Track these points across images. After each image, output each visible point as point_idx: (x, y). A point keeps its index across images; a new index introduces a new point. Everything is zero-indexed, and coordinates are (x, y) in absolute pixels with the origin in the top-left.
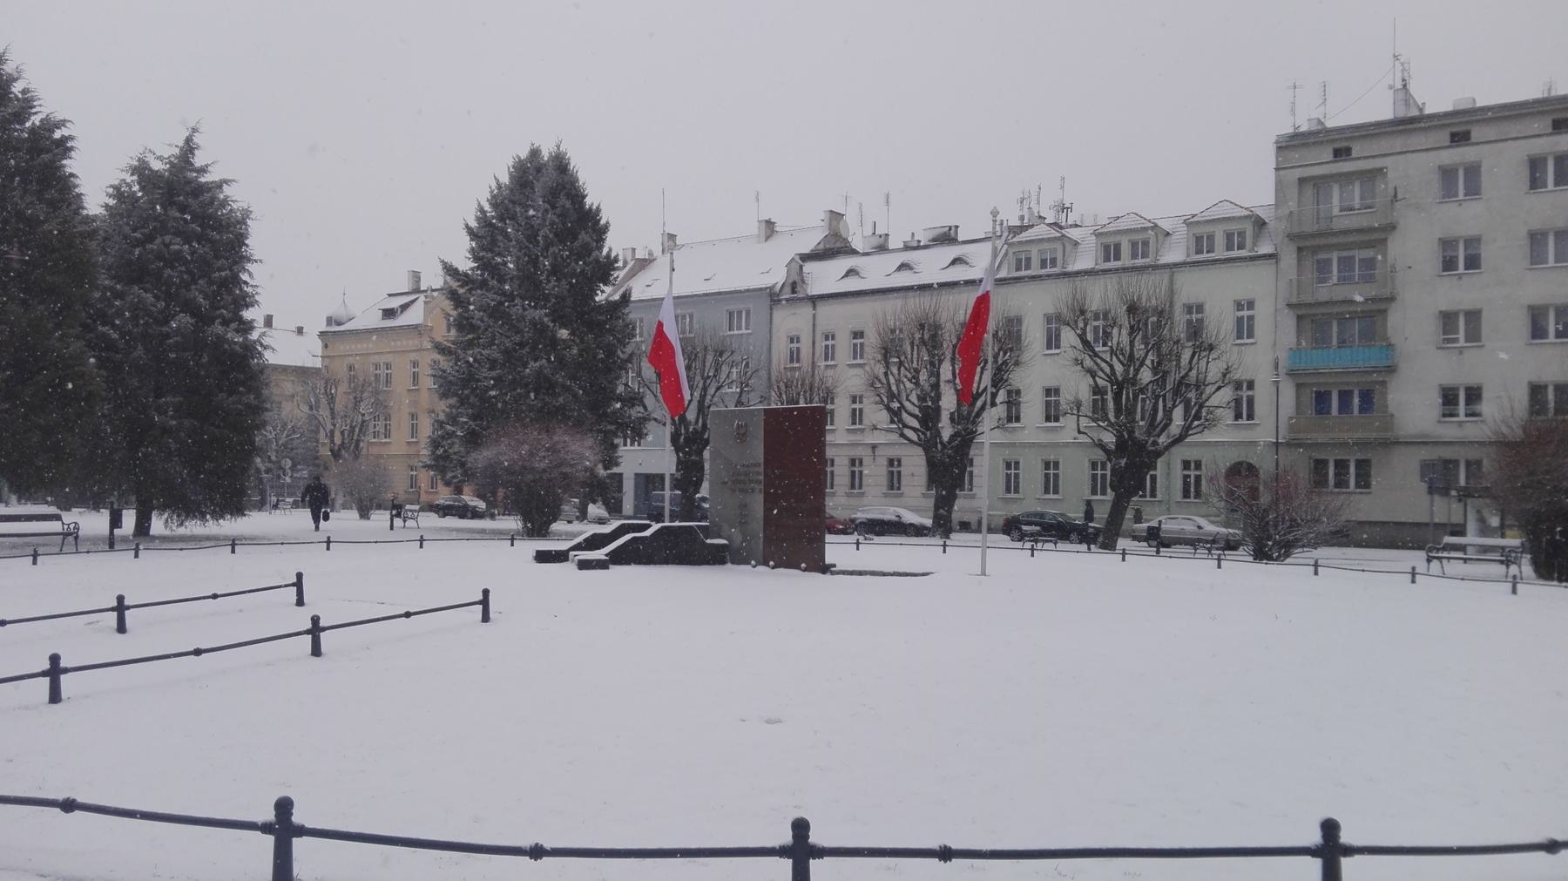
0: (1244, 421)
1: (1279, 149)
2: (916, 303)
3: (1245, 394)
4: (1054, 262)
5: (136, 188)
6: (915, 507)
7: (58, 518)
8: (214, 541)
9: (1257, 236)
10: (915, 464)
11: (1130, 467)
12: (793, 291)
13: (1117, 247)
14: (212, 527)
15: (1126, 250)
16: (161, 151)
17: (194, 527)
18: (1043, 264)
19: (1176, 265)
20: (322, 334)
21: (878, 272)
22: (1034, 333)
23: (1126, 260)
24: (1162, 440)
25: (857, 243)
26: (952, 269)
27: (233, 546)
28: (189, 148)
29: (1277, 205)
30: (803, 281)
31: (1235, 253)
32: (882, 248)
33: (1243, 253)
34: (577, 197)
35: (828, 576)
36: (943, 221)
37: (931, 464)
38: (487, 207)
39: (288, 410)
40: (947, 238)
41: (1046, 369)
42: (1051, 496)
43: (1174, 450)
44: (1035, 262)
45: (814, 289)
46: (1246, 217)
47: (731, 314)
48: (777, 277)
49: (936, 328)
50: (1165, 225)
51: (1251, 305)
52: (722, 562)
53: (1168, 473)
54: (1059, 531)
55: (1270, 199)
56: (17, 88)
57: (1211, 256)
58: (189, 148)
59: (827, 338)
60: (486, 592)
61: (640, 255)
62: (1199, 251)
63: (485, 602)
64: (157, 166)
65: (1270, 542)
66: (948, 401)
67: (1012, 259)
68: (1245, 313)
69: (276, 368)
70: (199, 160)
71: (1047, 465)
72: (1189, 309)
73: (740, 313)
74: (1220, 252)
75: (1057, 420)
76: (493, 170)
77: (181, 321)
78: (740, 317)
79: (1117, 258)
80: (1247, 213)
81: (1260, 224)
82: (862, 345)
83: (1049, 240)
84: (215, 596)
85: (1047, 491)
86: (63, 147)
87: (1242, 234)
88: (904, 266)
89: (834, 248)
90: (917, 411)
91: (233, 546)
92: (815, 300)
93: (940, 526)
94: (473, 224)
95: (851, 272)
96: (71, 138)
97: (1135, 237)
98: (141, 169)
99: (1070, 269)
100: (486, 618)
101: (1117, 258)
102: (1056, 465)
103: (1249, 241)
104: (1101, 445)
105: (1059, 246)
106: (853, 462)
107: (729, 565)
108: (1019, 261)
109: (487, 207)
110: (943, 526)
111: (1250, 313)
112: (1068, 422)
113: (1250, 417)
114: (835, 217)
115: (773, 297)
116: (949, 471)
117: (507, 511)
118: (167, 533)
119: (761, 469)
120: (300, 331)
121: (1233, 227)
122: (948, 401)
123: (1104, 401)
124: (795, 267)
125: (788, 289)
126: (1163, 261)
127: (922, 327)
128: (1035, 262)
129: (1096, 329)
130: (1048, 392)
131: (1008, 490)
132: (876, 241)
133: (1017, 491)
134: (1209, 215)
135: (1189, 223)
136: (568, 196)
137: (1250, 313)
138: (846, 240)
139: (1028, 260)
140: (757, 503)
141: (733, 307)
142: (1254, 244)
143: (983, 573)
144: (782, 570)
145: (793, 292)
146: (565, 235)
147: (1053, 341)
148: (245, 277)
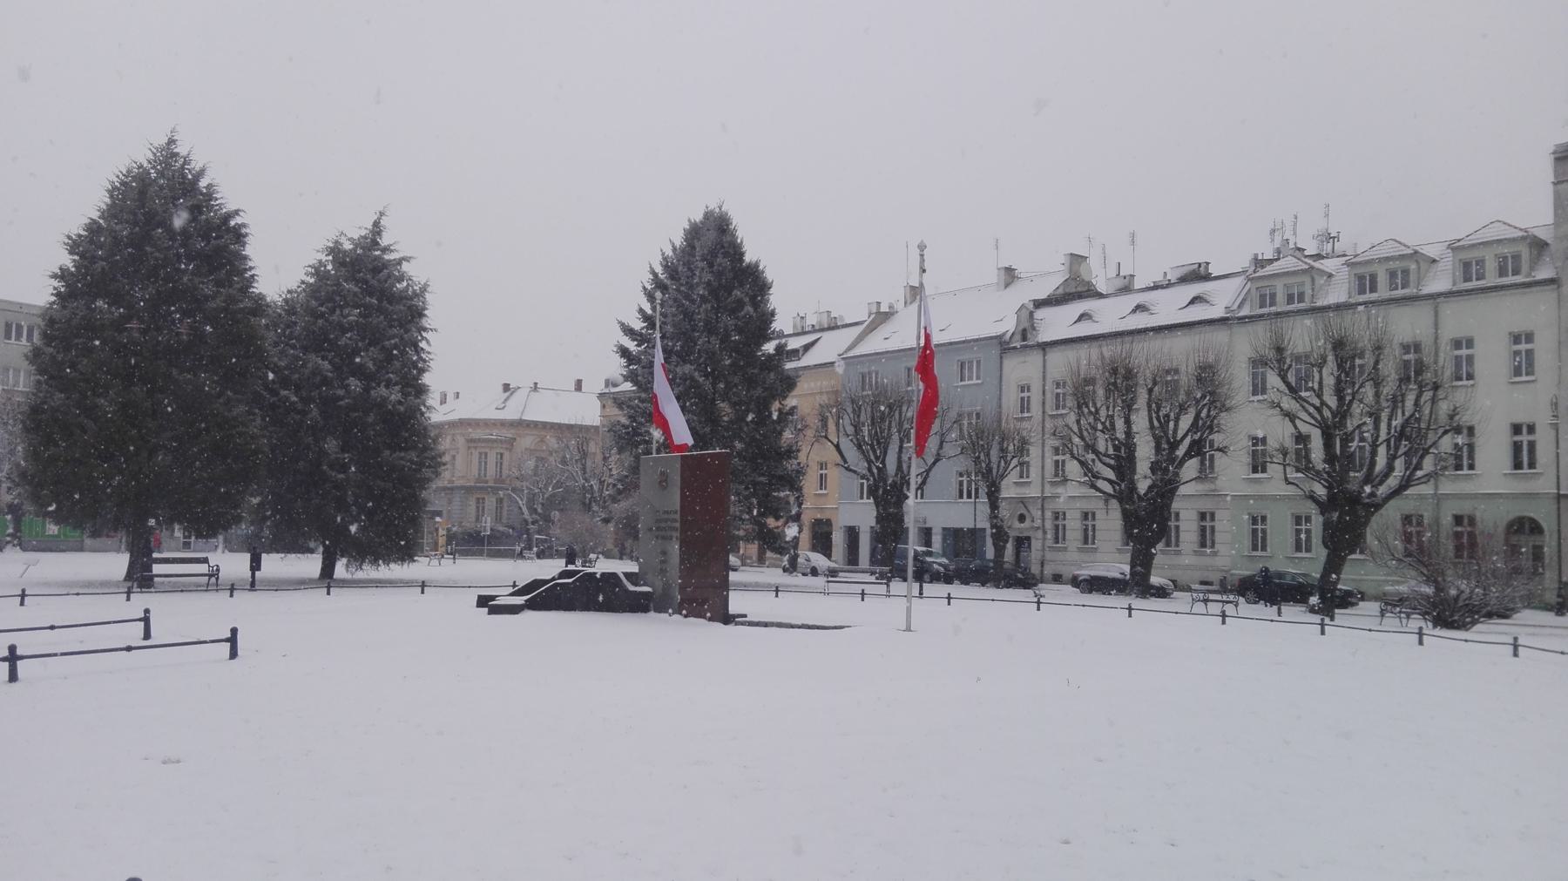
0: (1465, 472)
1: (1557, 159)
2: (1109, 350)
3: (1524, 438)
4: (1301, 298)
5: (330, 267)
6: (1119, 567)
7: (205, 561)
8: (407, 584)
9: (1535, 262)
10: (1111, 522)
11: (1345, 518)
12: (1024, 338)
13: (1373, 278)
14: (396, 571)
15: (1382, 280)
16: (354, 229)
17: (369, 572)
18: (1290, 299)
19: (1440, 295)
20: (601, 396)
21: (1111, 315)
22: (1239, 376)
23: (1383, 292)
24: (1382, 490)
25: (1102, 287)
26: (1192, 308)
27: (777, 591)
28: (377, 229)
29: (1557, 224)
30: (1034, 329)
31: (1510, 279)
32: (1126, 289)
33: (1519, 279)
34: (736, 252)
35: (731, 628)
36: (1191, 258)
37: (1126, 515)
38: (659, 270)
39: (459, 466)
40: (1197, 275)
41: (1252, 419)
42: (1303, 555)
43: (1392, 503)
44: (1281, 297)
45: (1045, 336)
46: (1523, 238)
48: (1008, 325)
49: (1130, 375)
50: (1431, 252)
51: (1529, 338)
52: (645, 610)
53: (1384, 525)
54: (1269, 590)
55: (1549, 218)
56: (203, 183)
57: (1481, 283)
58: (377, 229)
59: (1058, 385)
60: (234, 631)
61: (884, 308)
62: (1467, 279)
63: (233, 640)
64: (348, 246)
65: (1449, 614)
66: (1145, 452)
67: (1255, 295)
68: (1464, 352)
69: (440, 426)
70: (385, 241)
72: (1457, 344)
73: (971, 362)
74: (1492, 279)
75: (1264, 470)
76: (662, 236)
77: (354, 384)
78: (970, 369)
79: (1373, 289)
80: (1521, 234)
81: (1539, 246)
83: (1294, 273)
84: (52, 628)
85: (1255, 548)
86: (239, 235)
87: (1516, 257)
88: (1140, 308)
89: (1076, 290)
90: (1112, 462)
91: (777, 591)
92: (1044, 347)
93: (1137, 584)
95: (1084, 317)
96: (244, 225)
97: (1392, 265)
98: (335, 250)
99: (1319, 304)
100: (234, 654)
101: (1373, 289)
102: (1264, 519)
103: (1525, 267)
104: (1312, 497)
105: (1307, 280)
107: (652, 614)
108: (1263, 297)
109: (659, 270)
110: (1138, 584)
112: (1274, 470)
113: (1532, 465)
114: (1076, 259)
115: (1003, 345)
116: (1148, 523)
118: (348, 576)
119: (678, 516)
120: (579, 386)
121: (1506, 250)
122: (1145, 452)
123: (1308, 451)
124: (1025, 314)
125: (1018, 337)
126: (1426, 290)
127: (1114, 371)
128: (1281, 297)
129: (1298, 371)
130: (1517, 429)
131: (1255, 548)
132: (1120, 283)
133: (1264, 548)
134: (1476, 239)
135: (1454, 247)
136: (726, 255)
138: (1089, 283)
139: (1273, 296)
140: (675, 548)
141: (965, 357)
142: (1532, 269)
143: (908, 629)
144: (692, 619)
145: (1023, 340)
146: (718, 292)
147: (1259, 387)
148: (423, 345)
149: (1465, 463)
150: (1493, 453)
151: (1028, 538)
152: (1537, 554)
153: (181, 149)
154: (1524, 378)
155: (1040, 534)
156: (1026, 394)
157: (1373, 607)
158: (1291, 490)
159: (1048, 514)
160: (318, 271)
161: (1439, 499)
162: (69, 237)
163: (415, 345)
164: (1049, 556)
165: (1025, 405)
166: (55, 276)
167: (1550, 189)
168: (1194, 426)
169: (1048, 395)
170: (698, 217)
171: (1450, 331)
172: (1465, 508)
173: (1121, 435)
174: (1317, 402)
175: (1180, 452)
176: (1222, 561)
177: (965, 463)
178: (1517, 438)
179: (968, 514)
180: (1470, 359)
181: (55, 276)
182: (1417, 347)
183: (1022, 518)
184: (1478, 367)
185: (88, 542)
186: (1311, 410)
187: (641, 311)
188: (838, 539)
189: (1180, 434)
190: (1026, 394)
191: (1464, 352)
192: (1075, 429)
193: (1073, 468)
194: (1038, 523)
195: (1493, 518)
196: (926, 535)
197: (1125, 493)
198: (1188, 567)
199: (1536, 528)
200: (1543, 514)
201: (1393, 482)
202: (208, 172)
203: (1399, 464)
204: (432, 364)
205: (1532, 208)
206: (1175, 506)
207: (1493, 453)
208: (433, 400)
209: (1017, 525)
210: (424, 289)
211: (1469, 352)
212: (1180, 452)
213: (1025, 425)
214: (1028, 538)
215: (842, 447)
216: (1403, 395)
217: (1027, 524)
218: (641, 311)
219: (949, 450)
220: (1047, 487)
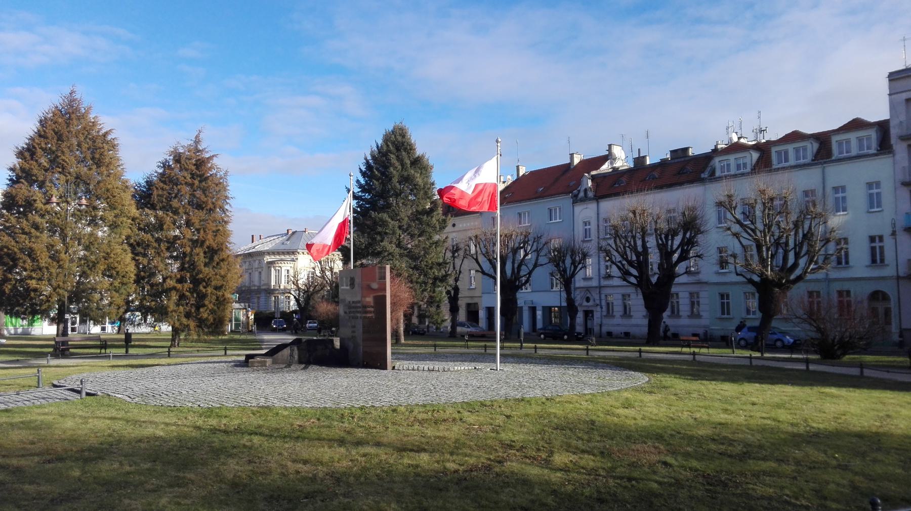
3: (877, 244)
10: (637, 302)
18: (738, 167)
22: (710, 216)
28: (197, 141)
38: (369, 158)
47: (551, 210)
51: (878, 184)
58: (197, 141)
59: (606, 221)
66: (654, 258)
68: (840, 195)
71: (722, 296)
72: (836, 189)
73: (556, 210)
79: (786, 160)
82: (878, 194)
94: (364, 169)
102: (728, 296)
111: (843, 195)
117: (815, 352)
122: (654, 258)
130: (872, 239)
131: (723, 313)
133: (728, 313)
137: (843, 195)
148: (227, 207)
149: (843, 261)
151: (592, 312)
152: (887, 312)
153: (77, 96)
154: (876, 210)
155: (599, 308)
157: (589, 322)
159: (603, 297)
161: (828, 280)
162: (17, 148)
164: (605, 321)
165: (587, 233)
167: (887, 98)
169: (601, 228)
171: (832, 182)
172: (846, 286)
173: (640, 249)
174: (753, 227)
176: (704, 322)
178: (873, 245)
179: (554, 298)
180: (844, 198)
183: (588, 300)
187: (358, 181)
188: (482, 314)
189: (675, 247)
190: (588, 227)
194: (598, 302)
195: (861, 292)
196: (533, 310)
197: (643, 283)
199: (885, 297)
200: (888, 288)
201: (798, 272)
205: (877, 109)
206: (674, 289)
207: (859, 254)
209: (585, 303)
210: (226, 173)
213: (588, 244)
214: (592, 312)
217: (591, 303)
218: (358, 181)
220: (602, 280)
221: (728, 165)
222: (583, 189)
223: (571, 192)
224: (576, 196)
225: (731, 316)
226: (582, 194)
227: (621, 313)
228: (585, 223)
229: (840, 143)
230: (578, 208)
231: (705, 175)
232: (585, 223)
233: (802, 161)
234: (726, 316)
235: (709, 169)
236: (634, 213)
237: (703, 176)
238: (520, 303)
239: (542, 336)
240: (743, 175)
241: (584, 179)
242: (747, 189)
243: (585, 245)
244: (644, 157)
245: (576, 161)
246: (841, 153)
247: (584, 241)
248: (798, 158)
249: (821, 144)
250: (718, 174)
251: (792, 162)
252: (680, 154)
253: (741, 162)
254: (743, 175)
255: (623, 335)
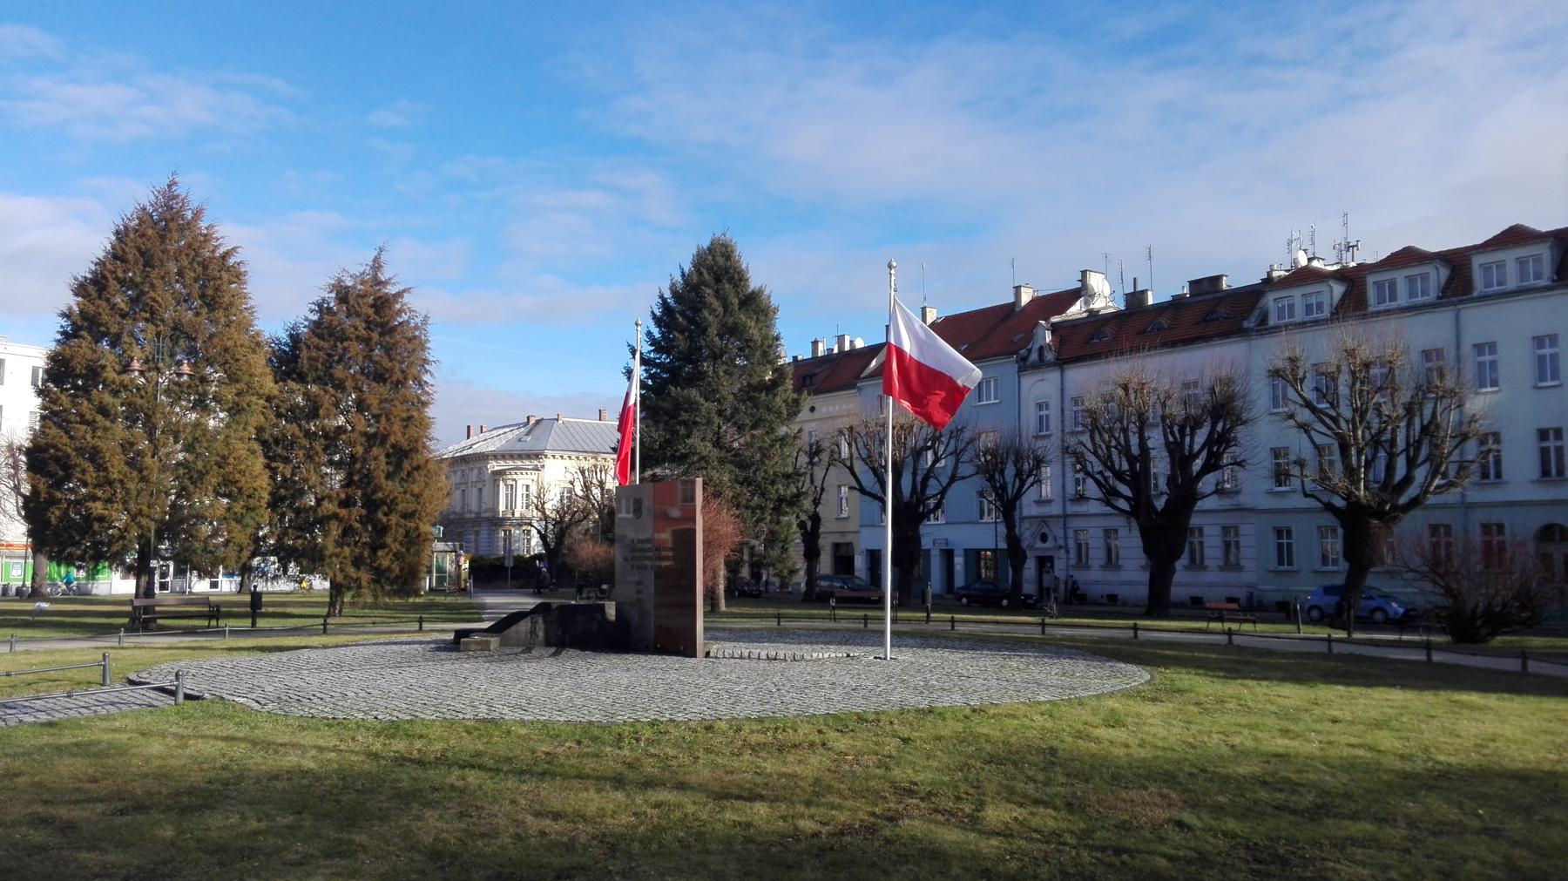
3: (1551, 444)
10: (1130, 543)
18: (1309, 309)
28: (377, 265)
38: (667, 295)
58: (377, 265)
66: (1160, 466)
68: (1487, 358)
72: (1479, 348)
79: (1393, 298)
86: (238, 276)
102: (1289, 532)
106: (1107, 531)
109: (667, 295)
122: (1160, 466)
130: (1543, 434)
131: (1281, 562)
133: (1290, 563)
148: (426, 378)
150: (1262, 464)
151: (1051, 559)
153: (179, 190)
154: (1549, 383)
155: (1062, 553)
156: (1044, 413)
158: (1313, 503)
159: (1070, 533)
160: (321, 308)
161: (1467, 507)
163: (417, 379)
165: (1042, 422)
166: (64, 315)
168: (1208, 443)
169: (1067, 413)
170: (706, 244)
172: (1496, 516)
173: (1135, 450)
175: (1198, 464)
177: (979, 482)
178: (1545, 444)
179: (986, 535)
180: (1493, 364)
181: (64, 315)
182: (1439, 353)
183: (1044, 538)
184: (1502, 371)
185: (1152, 809)
186: (1328, 421)
189: (1196, 447)
190: (1044, 413)
191: (1487, 358)
192: (1089, 445)
193: (1091, 489)
197: (1140, 509)
198: (1129, 583)
201: (1412, 491)
202: (206, 213)
203: (1420, 474)
204: (435, 396)
206: (1195, 521)
208: (436, 431)
209: (1039, 544)
211: (1552, 351)
212: (1198, 464)
213: (1046, 443)
214: (1051, 559)
215: (857, 470)
216: (1421, 405)
217: (1049, 544)
219: (965, 469)
221: (1291, 307)
222: (1037, 346)
223: (1016, 352)
224: (1024, 359)
225: (1295, 568)
226: (1034, 356)
227: (1102, 562)
228: (1040, 406)
229: (1486, 268)
230: (1028, 381)
231: (1249, 323)
232: (1040, 406)
233: (1420, 300)
234: (1285, 567)
235: (1256, 312)
236: (1125, 388)
237: (1246, 324)
238: (926, 543)
239: (1005, 602)
240: (1316, 322)
241: (1039, 330)
242: (1323, 348)
243: (1039, 443)
244: (1144, 292)
245: (1026, 298)
246: (1381, 301)
247: (1037, 437)
248: (1412, 294)
249: (1453, 269)
250: (1272, 321)
251: (1403, 300)
252: (1206, 287)
253: (1313, 300)
254: (1316, 322)
255: (1105, 600)
